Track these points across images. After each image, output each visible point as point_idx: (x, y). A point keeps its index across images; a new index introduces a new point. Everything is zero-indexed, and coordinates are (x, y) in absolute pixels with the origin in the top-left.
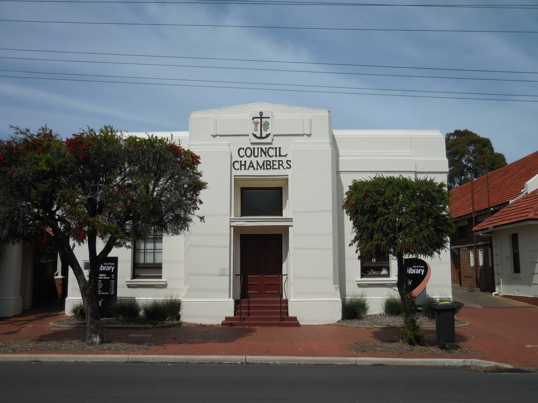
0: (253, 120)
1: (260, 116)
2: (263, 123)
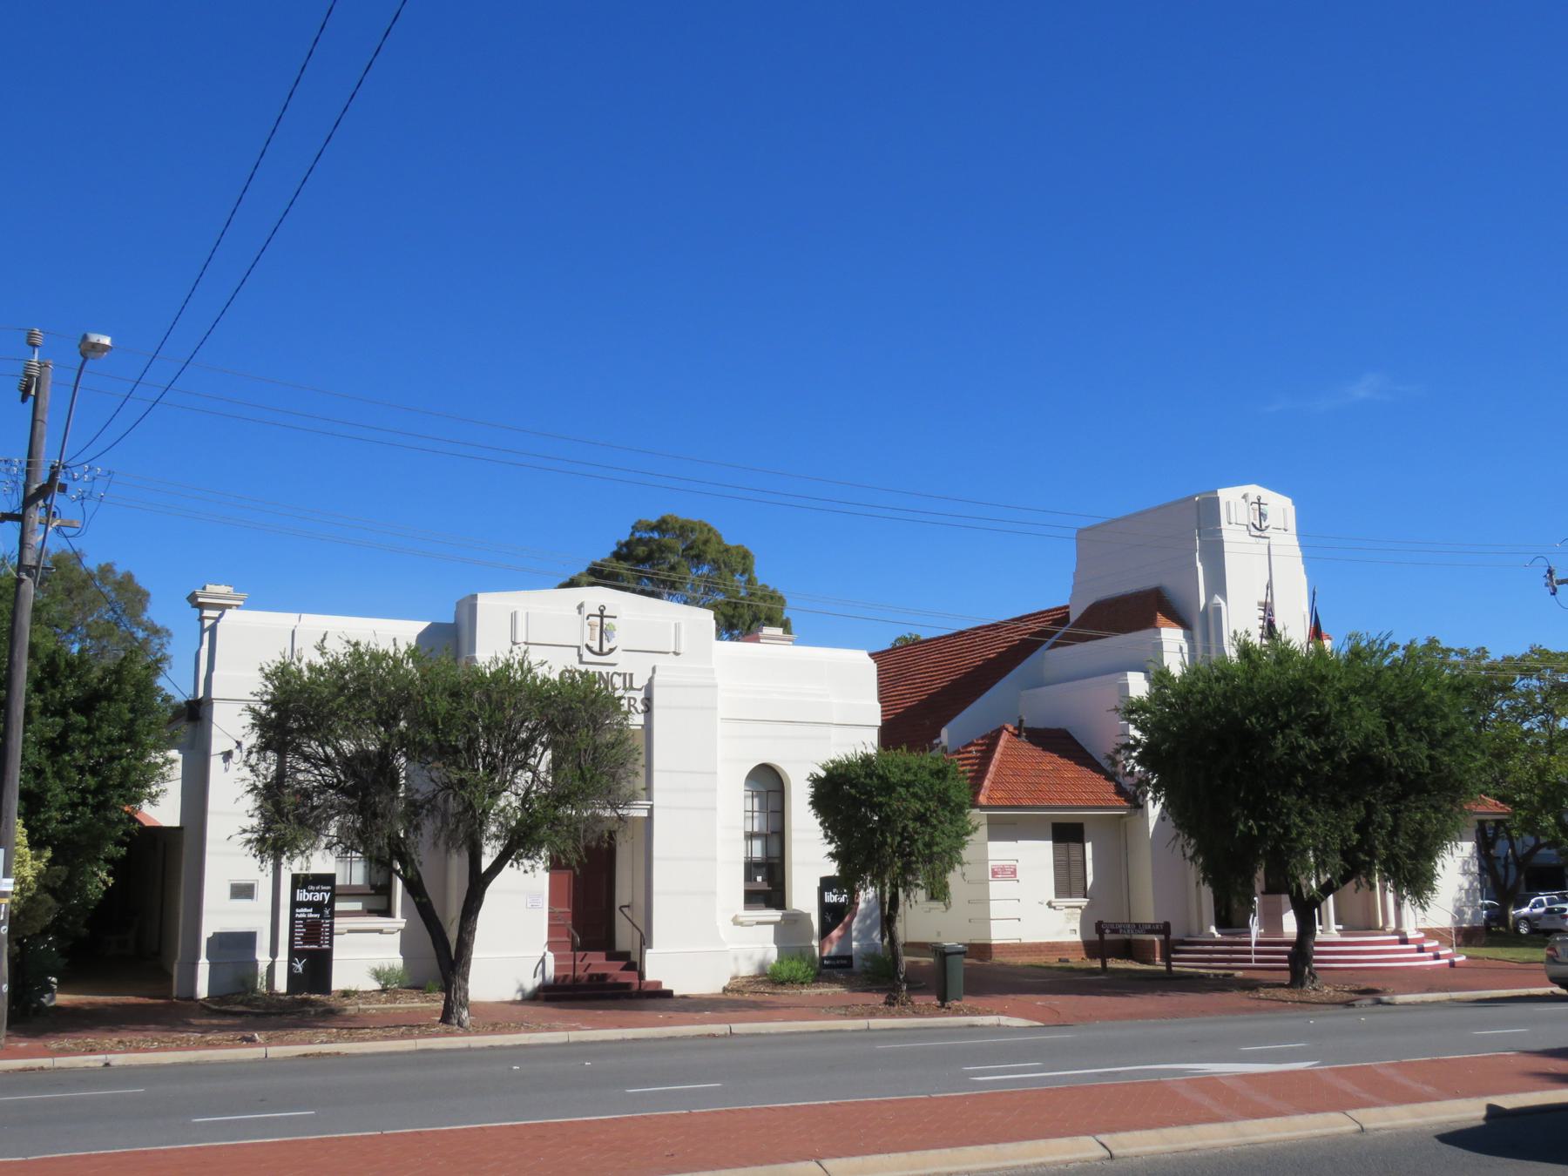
0: (588, 618)
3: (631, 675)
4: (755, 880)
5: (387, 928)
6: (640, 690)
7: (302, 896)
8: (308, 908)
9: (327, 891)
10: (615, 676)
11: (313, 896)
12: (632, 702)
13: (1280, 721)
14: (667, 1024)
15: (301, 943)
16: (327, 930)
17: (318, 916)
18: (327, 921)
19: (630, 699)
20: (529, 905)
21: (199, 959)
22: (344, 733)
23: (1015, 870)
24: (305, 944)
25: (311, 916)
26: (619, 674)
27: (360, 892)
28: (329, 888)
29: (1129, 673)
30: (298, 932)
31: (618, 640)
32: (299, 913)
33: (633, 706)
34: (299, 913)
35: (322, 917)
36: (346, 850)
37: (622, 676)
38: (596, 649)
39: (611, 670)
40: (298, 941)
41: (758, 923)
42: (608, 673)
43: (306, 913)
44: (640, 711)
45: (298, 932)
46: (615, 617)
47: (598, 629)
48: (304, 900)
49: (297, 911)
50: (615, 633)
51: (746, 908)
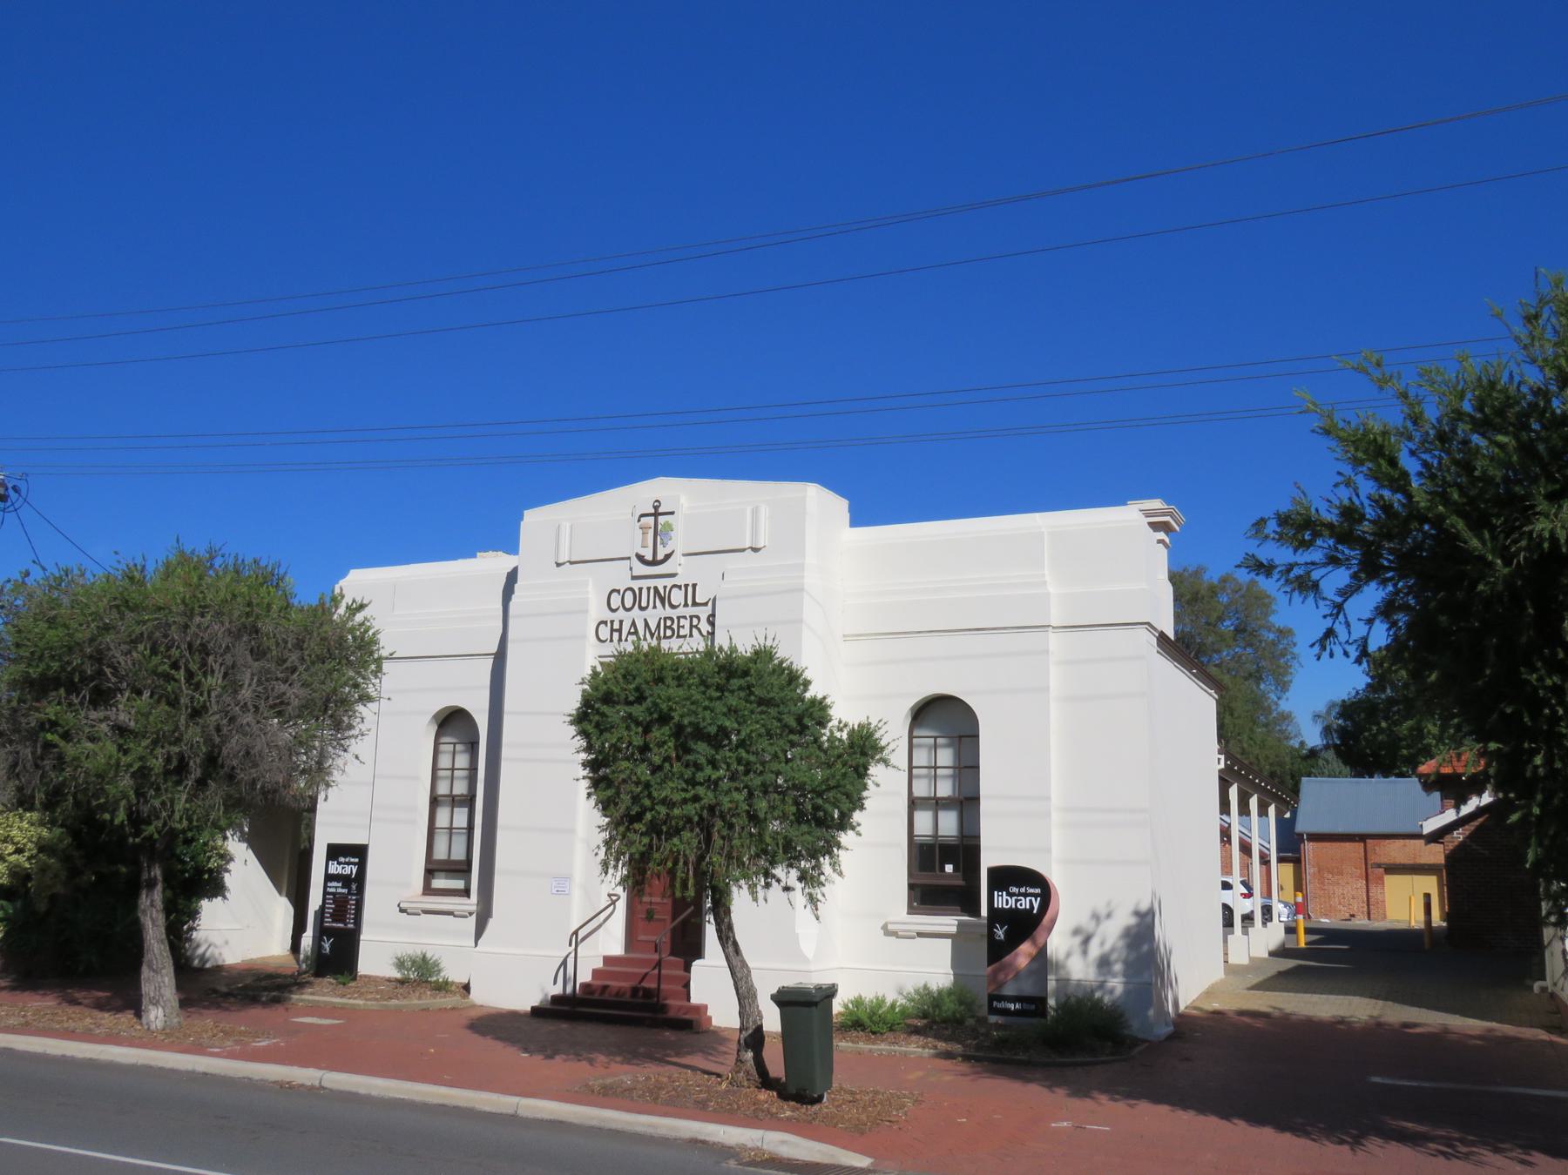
0: (639, 521)
1: (653, 511)
3: (694, 586)
4: (943, 869)
5: (458, 911)
6: (706, 604)
7: (334, 868)
8: (338, 882)
9: (354, 864)
10: (675, 590)
11: (343, 868)
12: (695, 621)
14: (88, 1036)
15: (330, 920)
16: (353, 907)
17: (345, 891)
18: (354, 898)
20: (554, 891)
21: (305, 932)
24: (334, 921)
25: (340, 890)
26: (680, 587)
27: (458, 867)
30: (329, 908)
31: (679, 542)
32: (330, 887)
33: (696, 627)
34: (330, 887)
35: (349, 893)
37: (683, 588)
38: (649, 557)
39: (669, 582)
40: (328, 918)
41: (920, 935)
42: (665, 587)
43: (336, 887)
45: (329, 908)
46: (672, 513)
47: (651, 532)
49: (329, 884)
50: (672, 534)
51: (912, 910)
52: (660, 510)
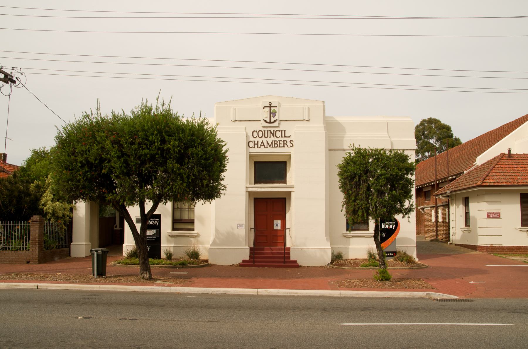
0: (264, 108)
1: (269, 106)
2: (271, 111)
3: (285, 131)
9: (157, 221)
12: (285, 142)
13: (121, 156)
19: (284, 141)
20: (238, 228)
22: (194, 147)
23: (500, 214)
26: (279, 131)
28: (158, 220)
29: (511, 153)
36: (198, 200)
37: (281, 131)
38: (268, 121)
39: (275, 129)
44: (289, 146)
48: (385, 227)
52: (272, 106)
